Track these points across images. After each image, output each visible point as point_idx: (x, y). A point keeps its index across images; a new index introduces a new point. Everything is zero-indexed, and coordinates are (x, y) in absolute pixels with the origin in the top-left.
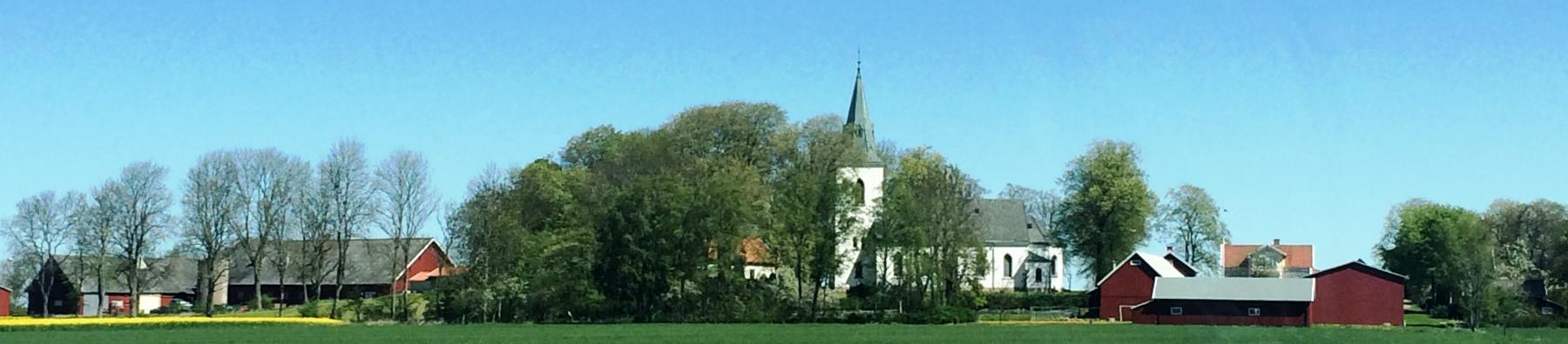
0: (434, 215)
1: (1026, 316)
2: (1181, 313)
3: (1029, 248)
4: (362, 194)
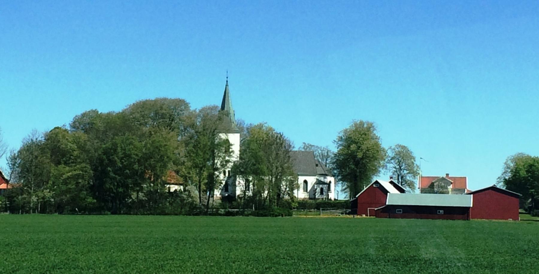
2: (402, 212)
3: (316, 177)
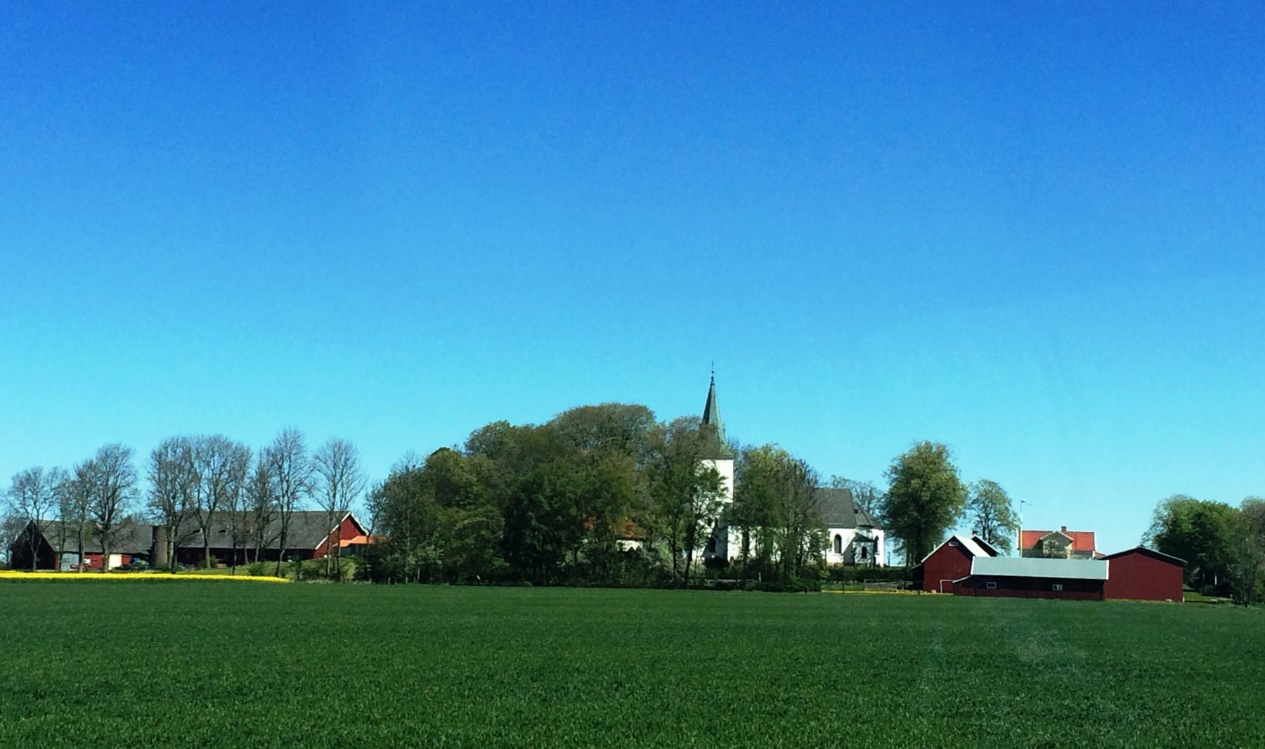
1: (860, 586)
3: (856, 530)
4: (302, 474)
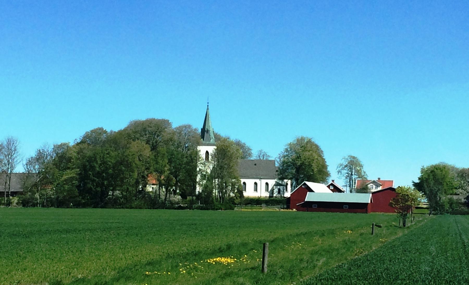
0: (21, 163)
2: (348, 208)
3: (276, 180)
